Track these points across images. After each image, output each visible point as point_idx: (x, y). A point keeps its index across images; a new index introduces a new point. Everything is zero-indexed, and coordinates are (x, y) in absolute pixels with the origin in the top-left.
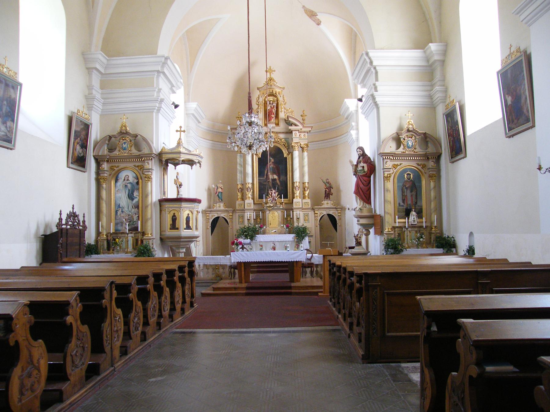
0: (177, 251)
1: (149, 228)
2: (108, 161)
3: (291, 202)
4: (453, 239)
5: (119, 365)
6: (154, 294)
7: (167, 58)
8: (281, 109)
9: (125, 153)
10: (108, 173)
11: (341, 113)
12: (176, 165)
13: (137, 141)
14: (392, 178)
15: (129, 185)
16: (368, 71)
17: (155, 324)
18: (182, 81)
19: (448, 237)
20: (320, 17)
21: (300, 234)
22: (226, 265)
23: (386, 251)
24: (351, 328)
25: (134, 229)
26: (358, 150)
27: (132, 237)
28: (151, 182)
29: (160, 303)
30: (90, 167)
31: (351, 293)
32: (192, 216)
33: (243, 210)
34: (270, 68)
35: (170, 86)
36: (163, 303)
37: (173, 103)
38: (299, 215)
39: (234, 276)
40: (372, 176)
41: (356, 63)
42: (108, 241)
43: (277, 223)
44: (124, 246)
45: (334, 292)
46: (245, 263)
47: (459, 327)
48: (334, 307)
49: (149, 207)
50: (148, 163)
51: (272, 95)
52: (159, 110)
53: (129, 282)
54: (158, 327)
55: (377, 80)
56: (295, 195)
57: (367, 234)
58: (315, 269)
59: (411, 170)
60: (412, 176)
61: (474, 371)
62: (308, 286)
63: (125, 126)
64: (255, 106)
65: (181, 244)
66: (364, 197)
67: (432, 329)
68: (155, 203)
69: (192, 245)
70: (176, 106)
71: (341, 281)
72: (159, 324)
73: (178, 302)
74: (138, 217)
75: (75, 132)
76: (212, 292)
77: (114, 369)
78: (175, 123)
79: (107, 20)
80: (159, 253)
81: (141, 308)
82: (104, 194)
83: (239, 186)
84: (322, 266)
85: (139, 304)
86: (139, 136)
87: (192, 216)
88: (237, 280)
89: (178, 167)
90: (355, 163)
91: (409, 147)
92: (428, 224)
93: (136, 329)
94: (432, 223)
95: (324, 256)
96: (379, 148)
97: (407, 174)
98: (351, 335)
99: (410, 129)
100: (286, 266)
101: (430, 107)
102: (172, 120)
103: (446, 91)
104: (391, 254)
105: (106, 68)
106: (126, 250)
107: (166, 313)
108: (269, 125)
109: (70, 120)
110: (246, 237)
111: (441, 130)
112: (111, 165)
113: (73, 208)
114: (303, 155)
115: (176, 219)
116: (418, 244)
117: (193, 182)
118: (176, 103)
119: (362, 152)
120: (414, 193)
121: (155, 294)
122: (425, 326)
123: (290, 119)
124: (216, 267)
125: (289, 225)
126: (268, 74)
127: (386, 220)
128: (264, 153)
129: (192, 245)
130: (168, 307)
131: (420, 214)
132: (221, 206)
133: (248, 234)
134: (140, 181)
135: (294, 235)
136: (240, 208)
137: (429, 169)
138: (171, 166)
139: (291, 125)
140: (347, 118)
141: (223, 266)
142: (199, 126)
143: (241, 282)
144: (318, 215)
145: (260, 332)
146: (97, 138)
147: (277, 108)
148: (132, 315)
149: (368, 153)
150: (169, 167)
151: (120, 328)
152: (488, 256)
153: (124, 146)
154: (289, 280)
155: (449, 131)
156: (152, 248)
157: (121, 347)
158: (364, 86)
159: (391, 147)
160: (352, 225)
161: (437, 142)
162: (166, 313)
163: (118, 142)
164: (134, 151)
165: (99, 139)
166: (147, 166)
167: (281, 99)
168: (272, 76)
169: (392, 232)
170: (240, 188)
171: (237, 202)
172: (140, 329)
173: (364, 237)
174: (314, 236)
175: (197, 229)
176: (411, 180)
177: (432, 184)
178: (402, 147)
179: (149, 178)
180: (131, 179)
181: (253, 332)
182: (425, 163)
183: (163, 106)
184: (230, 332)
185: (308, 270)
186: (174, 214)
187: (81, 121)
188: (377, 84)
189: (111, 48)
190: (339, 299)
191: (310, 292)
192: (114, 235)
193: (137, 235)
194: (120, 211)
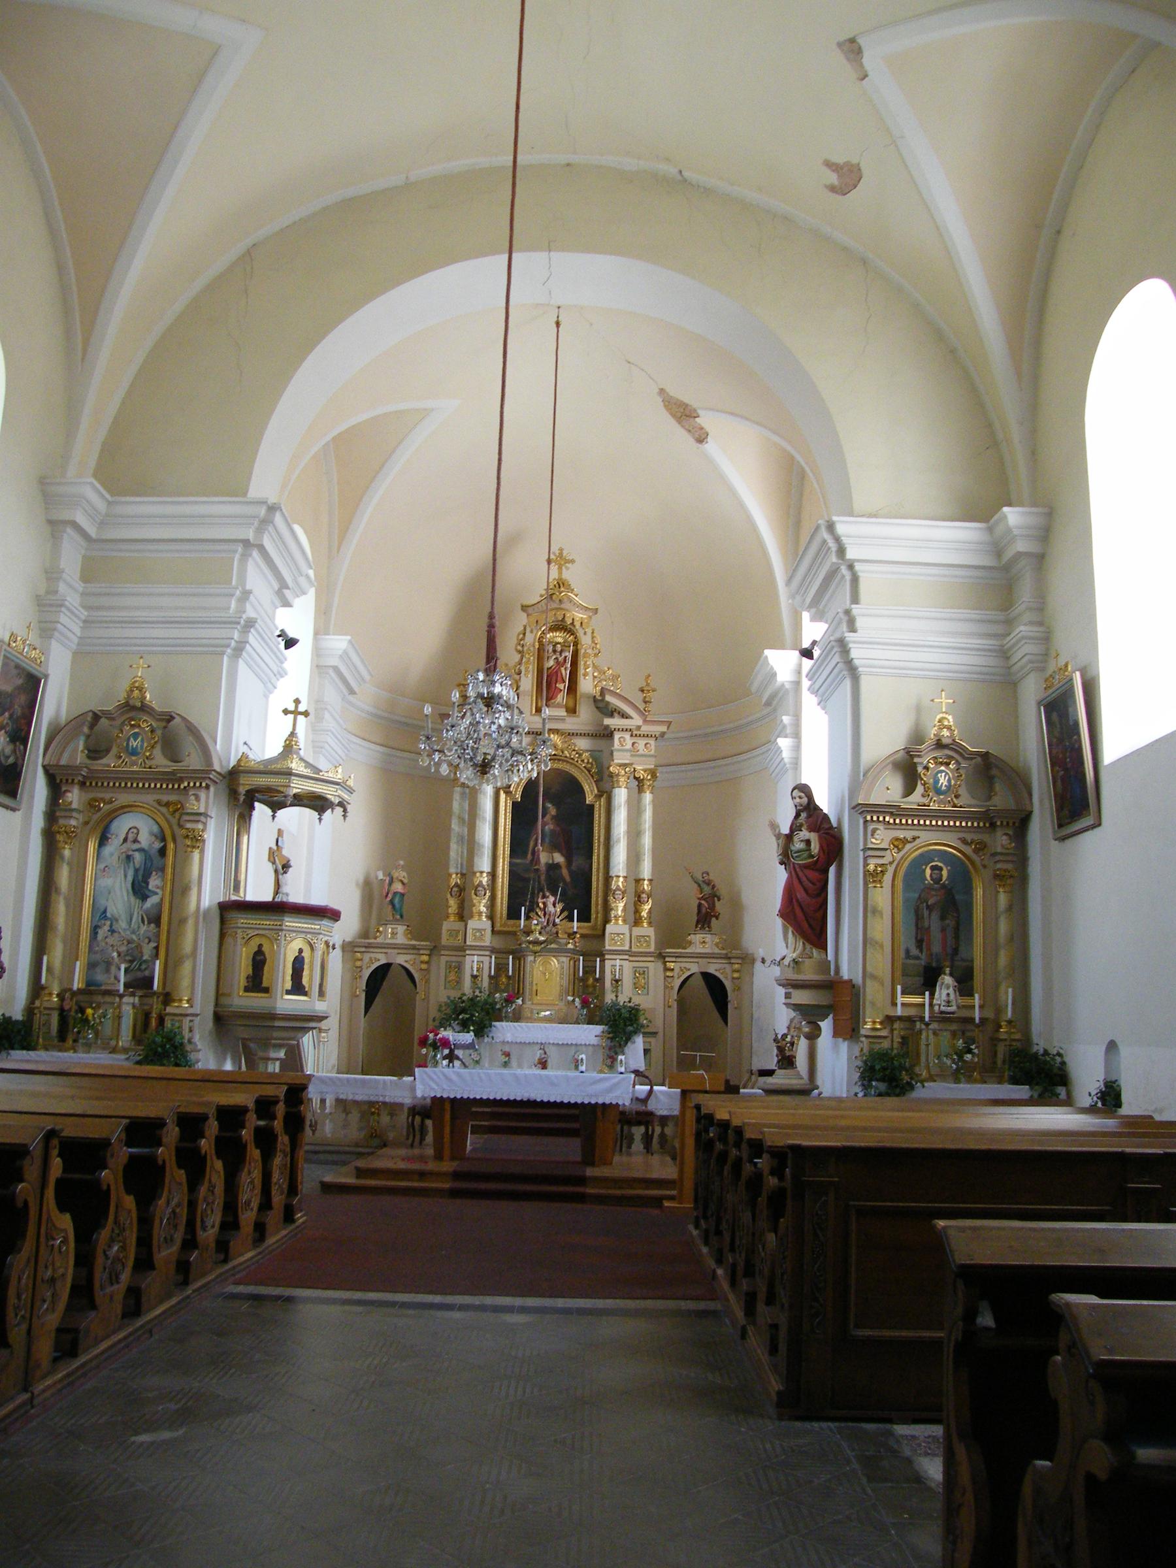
0: (261, 1054)
1: (185, 983)
2: (82, 784)
3: (600, 933)
4: (1058, 1059)
5: (49, 1387)
6: (176, 1176)
7: (273, 509)
8: (586, 667)
9: (134, 763)
10: (81, 817)
11: (754, 689)
12: (276, 807)
13: (172, 732)
14: (888, 877)
16: (832, 577)
17: (173, 1267)
18: (311, 573)
19: (1046, 1053)
20: (705, 420)
21: (621, 1025)
22: (402, 1105)
23: (866, 1087)
24: (750, 1311)
25: (141, 984)
26: (796, 793)
27: (134, 1006)
28: (202, 852)
29: (192, 1205)
30: (32, 797)
31: (753, 1203)
32: (312, 957)
33: (462, 949)
34: (561, 554)
35: (276, 586)
36: (202, 1206)
37: (282, 634)
39: (422, 1139)
40: (832, 870)
41: (802, 549)
42: (62, 1011)
43: (556, 990)
44: (107, 1029)
45: (706, 1202)
46: (454, 1101)
47: (1057, 1319)
48: (706, 1243)
50: (197, 798)
52: (239, 650)
53: (104, 1136)
54: (180, 1278)
55: (855, 599)
56: (613, 914)
57: (813, 1036)
58: (658, 1130)
60: (945, 873)
61: (1099, 1459)
62: (635, 1180)
63: (140, 689)
64: (507, 654)
65: (275, 1034)
67: (979, 1320)
68: (207, 912)
69: (307, 1040)
70: (290, 643)
71: (727, 1169)
72: (184, 1270)
73: (248, 1203)
74: (157, 948)
76: (351, 1180)
77: (32, 1398)
78: (284, 690)
80: (206, 1057)
81: (134, 1215)
82: (63, 876)
83: (455, 879)
84: (679, 1120)
85: (129, 1202)
86: (177, 720)
87: (312, 957)
88: (430, 1151)
89: (281, 813)
90: (785, 830)
91: (938, 792)
92: (990, 1014)
93: (114, 1278)
94: (999, 1011)
95: (684, 1093)
96: (855, 785)
97: (933, 868)
98: (750, 1330)
99: (945, 741)
100: (575, 1118)
101: (1002, 680)
102: (274, 680)
103: (1046, 639)
104: (880, 1095)
105: (102, 524)
106: (113, 1043)
107: (209, 1234)
108: (547, 712)
110: (464, 1026)
111: (1032, 747)
112: (92, 795)
114: (639, 801)
115: (263, 962)
116: (958, 1070)
117: (321, 858)
118: (291, 634)
119: (805, 800)
120: (950, 922)
121: (181, 1175)
122: (960, 1310)
123: (608, 698)
124: (371, 1109)
125: (588, 998)
126: (554, 568)
127: (869, 998)
128: (530, 787)
129: (307, 1040)
130: (215, 1219)
131: (965, 984)
133: (470, 1019)
134: (171, 846)
137: (994, 855)
138: (261, 811)
139: (611, 715)
140: (768, 703)
141: (393, 1108)
142: (353, 705)
143: (439, 1156)
144: (675, 974)
145: (483, 1308)
147: (575, 664)
148: (104, 1234)
149: (823, 801)
150: (255, 814)
151: (61, 1271)
152: (1161, 1111)
153: (134, 743)
154: (579, 1159)
155: (1054, 751)
156: (190, 1041)
157: (59, 1331)
158: (818, 617)
159: (889, 789)
160: (771, 1007)
161: (1019, 781)
162: (209, 1234)
163: (115, 732)
164: (160, 761)
165: (63, 719)
166: (193, 805)
167: (585, 641)
168: (566, 575)
169: (884, 1033)
170: (456, 885)
171: (446, 926)
172: (125, 1277)
173: (802, 1046)
174: (661, 1034)
175: (322, 993)
176: (944, 886)
177: (1003, 899)
178: (920, 789)
179: (197, 841)
180: (145, 839)
181: (462, 1308)
182: (986, 837)
183: (251, 639)
184: (393, 1304)
185: (638, 1131)
186: (260, 946)
187: (17, 667)
188: (856, 610)
189: (122, 472)
190: (719, 1221)
191: (639, 1197)
192: (81, 998)
193: (149, 1000)
194: (106, 928)
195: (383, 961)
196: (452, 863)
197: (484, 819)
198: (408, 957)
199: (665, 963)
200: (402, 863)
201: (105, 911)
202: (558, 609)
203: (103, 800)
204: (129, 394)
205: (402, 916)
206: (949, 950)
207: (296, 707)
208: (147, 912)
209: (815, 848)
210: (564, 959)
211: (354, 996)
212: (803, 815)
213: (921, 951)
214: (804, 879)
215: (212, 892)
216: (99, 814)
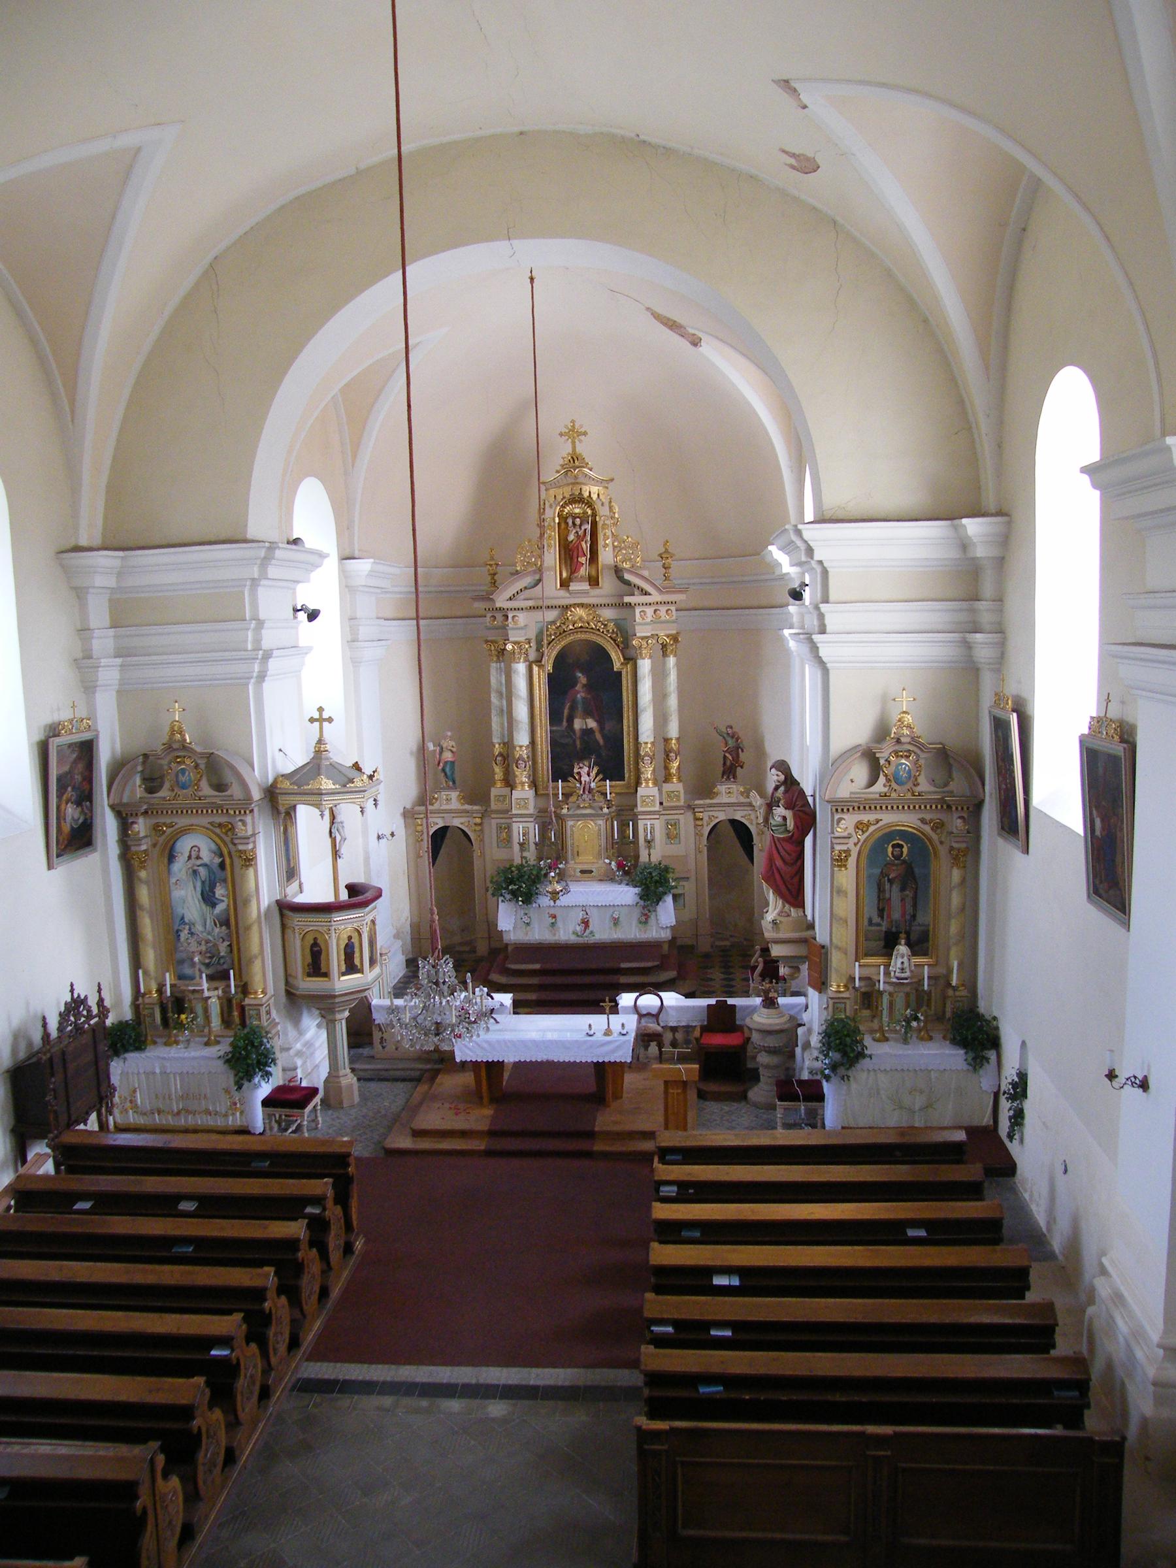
15: (201, 869)
27: (219, 997)
30: (105, 836)
38: (652, 828)
40: (808, 841)
49: (255, 928)
51: (578, 499)
52: (262, 677)
59: (903, 835)
60: (905, 850)
66: (784, 889)
70: (313, 616)
74: (230, 945)
75: (59, 780)
79: (112, 443)
82: (144, 895)
97: (893, 846)
109: (43, 751)
113: (72, 991)
114: (664, 664)
115: (320, 952)
125: (627, 863)
132: (451, 800)
134: (228, 861)
135: (637, 890)
136: (500, 806)
146: (113, 749)
167: (603, 511)
170: (501, 754)
171: (494, 792)
176: (904, 862)
179: (249, 861)
180: (206, 856)
182: (942, 816)
186: (315, 939)
194: (186, 932)
195: (441, 824)
196: (494, 733)
197: (519, 697)
198: (463, 820)
199: (694, 813)
200: (449, 734)
201: (183, 918)
202: (573, 484)
203: (164, 824)
204: (122, 430)
205: (454, 782)
206: (908, 917)
207: (321, 715)
208: (218, 916)
209: (791, 824)
210: (600, 822)
211: (419, 856)
212: (782, 789)
213: (882, 918)
214: (781, 850)
215: (269, 891)
216: (164, 837)
